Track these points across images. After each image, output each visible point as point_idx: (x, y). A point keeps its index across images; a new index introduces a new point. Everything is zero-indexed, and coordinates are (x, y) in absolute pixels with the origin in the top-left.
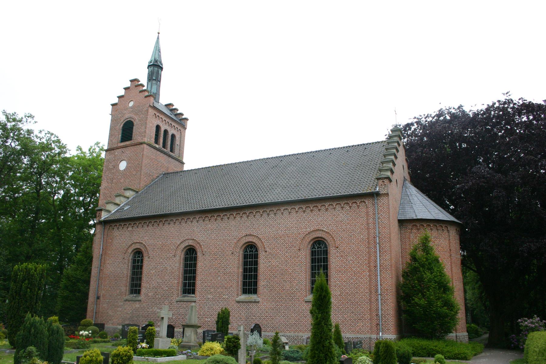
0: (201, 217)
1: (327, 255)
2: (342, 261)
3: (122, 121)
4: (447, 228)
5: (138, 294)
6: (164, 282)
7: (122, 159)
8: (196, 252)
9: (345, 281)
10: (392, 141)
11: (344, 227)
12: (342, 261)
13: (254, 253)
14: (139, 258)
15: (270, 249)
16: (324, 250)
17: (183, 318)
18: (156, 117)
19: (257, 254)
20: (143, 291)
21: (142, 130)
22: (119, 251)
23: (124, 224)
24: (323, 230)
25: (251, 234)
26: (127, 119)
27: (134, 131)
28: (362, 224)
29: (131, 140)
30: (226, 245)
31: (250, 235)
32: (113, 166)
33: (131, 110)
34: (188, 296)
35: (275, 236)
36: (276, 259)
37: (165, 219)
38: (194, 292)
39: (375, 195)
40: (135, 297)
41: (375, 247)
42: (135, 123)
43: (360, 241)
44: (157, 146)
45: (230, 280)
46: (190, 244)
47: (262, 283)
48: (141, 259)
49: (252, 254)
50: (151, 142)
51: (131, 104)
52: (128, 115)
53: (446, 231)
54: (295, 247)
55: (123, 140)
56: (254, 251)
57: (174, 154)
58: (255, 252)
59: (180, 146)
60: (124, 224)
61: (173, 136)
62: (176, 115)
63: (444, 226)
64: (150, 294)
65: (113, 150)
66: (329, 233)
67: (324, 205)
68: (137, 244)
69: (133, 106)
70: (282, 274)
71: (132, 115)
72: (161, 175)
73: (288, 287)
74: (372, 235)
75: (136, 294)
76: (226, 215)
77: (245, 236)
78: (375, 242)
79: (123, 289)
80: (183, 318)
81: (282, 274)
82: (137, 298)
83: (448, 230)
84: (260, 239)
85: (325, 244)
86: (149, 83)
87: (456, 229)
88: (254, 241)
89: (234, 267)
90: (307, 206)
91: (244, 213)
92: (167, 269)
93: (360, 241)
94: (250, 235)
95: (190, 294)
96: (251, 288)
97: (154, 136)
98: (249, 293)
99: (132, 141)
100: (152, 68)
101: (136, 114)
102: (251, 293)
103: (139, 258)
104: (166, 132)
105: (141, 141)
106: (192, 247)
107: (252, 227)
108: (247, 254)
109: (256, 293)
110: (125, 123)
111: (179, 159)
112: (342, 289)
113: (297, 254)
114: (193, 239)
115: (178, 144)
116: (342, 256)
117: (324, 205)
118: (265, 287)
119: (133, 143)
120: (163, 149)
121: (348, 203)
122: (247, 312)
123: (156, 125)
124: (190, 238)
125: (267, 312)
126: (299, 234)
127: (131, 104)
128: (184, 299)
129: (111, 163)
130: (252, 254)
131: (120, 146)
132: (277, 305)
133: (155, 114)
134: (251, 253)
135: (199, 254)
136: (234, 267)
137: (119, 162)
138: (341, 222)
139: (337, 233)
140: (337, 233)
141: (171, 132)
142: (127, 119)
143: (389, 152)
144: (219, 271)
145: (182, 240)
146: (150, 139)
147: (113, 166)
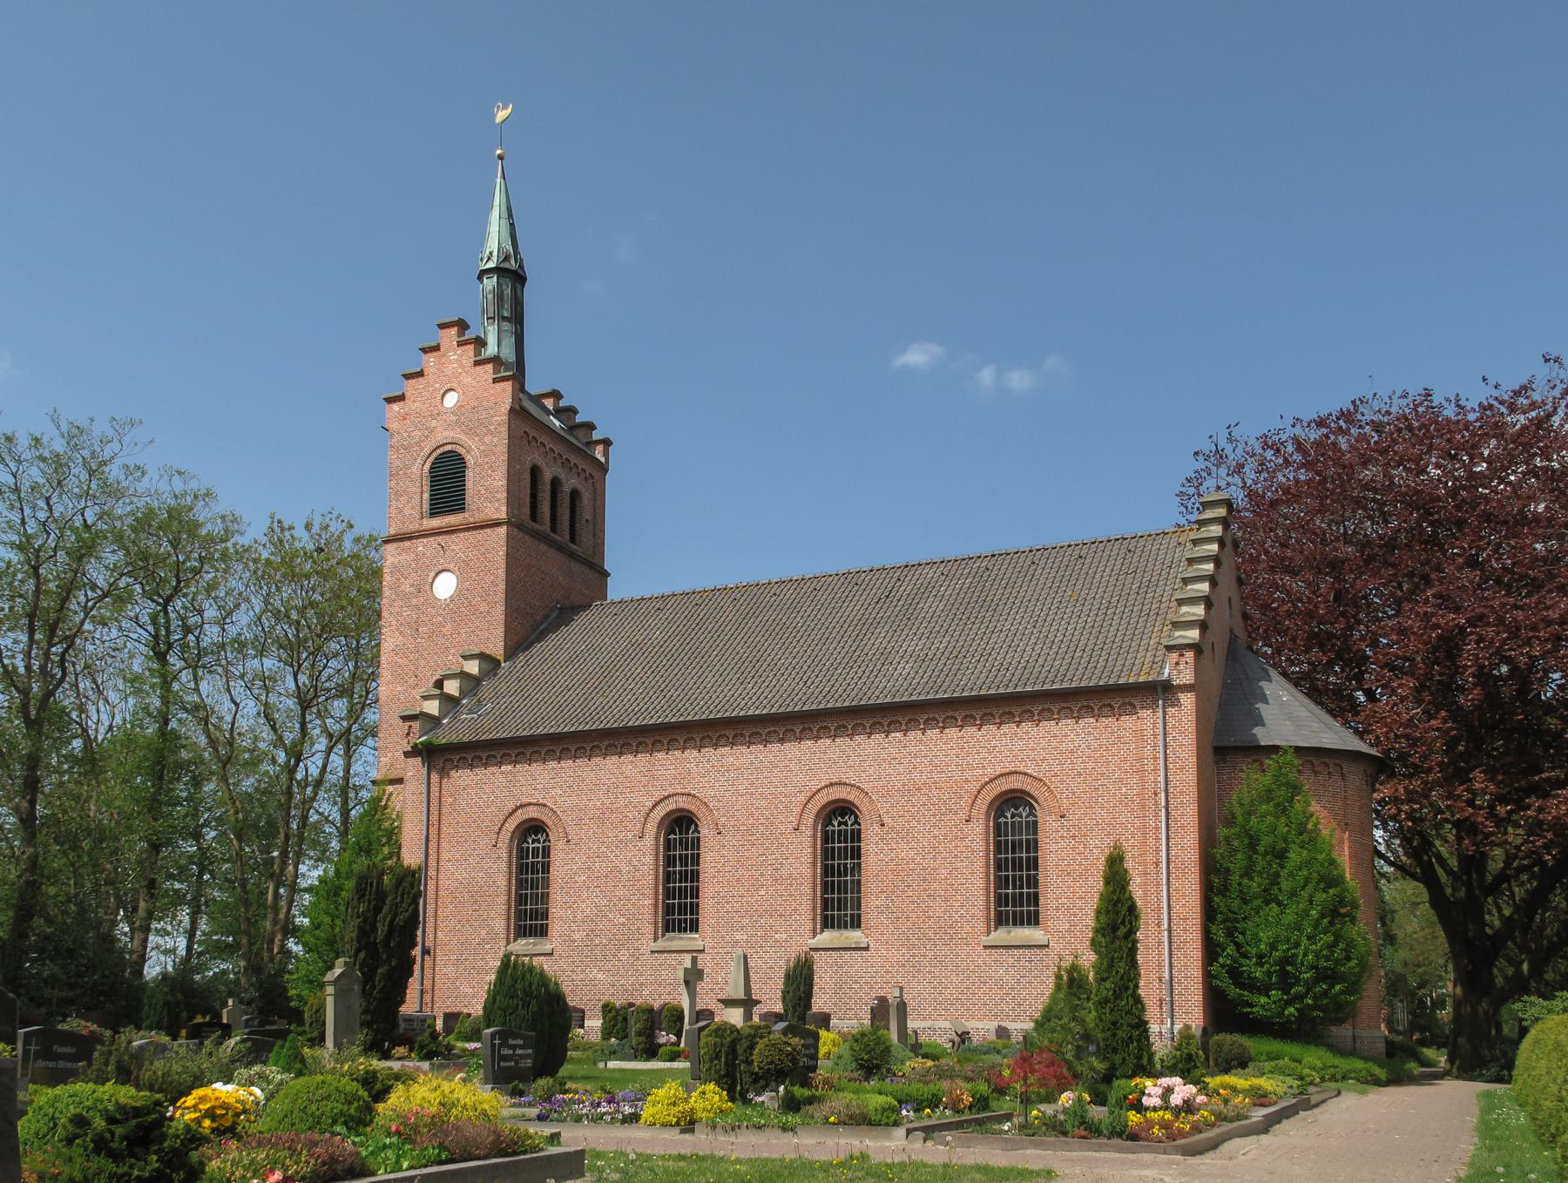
0: (708, 736)
1: (1035, 833)
2: (1073, 849)
3: (427, 450)
4: (1342, 769)
5: (541, 935)
6: (615, 905)
7: (440, 568)
8: (696, 826)
9: (1080, 898)
10: (1204, 535)
11: (1079, 767)
12: (1073, 849)
13: (849, 828)
14: (536, 845)
15: (893, 818)
16: (1027, 823)
17: (669, 993)
18: (529, 442)
19: (859, 831)
20: (556, 927)
21: (495, 483)
22: (478, 827)
23: (489, 756)
24: (1025, 774)
25: (844, 780)
26: (443, 445)
27: (469, 484)
28: (1125, 760)
29: (462, 510)
30: (776, 808)
31: (840, 784)
32: (412, 585)
33: (454, 418)
34: (681, 938)
35: (904, 785)
36: (908, 842)
37: (606, 743)
38: (694, 927)
39: (1159, 689)
40: (534, 944)
41: (1157, 816)
42: (470, 460)
43: (1121, 802)
44: (537, 526)
45: (791, 895)
46: (681, 805)
47: (872, 902)
48: (544, 848)
49: (846, 831)
50: (523, 517)
51: (451, 400)
52: (446, 434)
53: (1336, 777)
54: (956, 813)
55: (437, 509)
56: (849, 823)
57: (580, 550)
58: (852, 825)
59: (594, 524)
60: (489, 756)
61: (575, 495)
62: (573, 428)
63: (1331, 762)
64: (576, 936)
65: (410, 538)
66: (1041, 780)
67: (1029, 711)
68: (531, 808)
69: (458, 408)
70: (925, 880)
71: (450, 435)
72: (552, 610)
73: (939, 912)
74: (1150, 786)
75: (536, 935)
76: (775, 732)
77: (826, 786)
78: (1156, 804)
79: (500, 925)
80: (669, 993)
81: (925, 880)
82: (538, 947)
83: (1342, 774)
84: (867, 793)
85: (1032, 807)
86: (491, 328)
87: (1365, 771)
88: (851, 798)
89: (801, 863)
90: (985, 711)
91: (821, 728)
92: (620, 872)
93: (1121, 802)
94: (840, 784)
95: (685, 931)
96: (846, 915)
97: (528, 500)
98: (839, 927)
99: (466, 515)
100: (495, 279)
101: (470, 432)
102: (846, 927)
103: (536, 845)
104: (555, 483)
105: (495, 516)
106: (685, 814)
107: (845, 763)
108: (833, 831)
109: (859, 926)
110: (436, 459)
111: (595, 561)
112: (1075, 915)
113: (962, 830)
114: (689, 795)
115: (588, 516)
116: (1074, 837)
117: (1029, 711)
118: (882, 912)
119: (471, 520)
120: (551, 534)
121: (1091, 708)
122: (836, 973)
123: (531, 465)
124: (679, 791)
125: (887, 972)
126: (967, 781)
127: (451, 400)
128: (670, 946)
129: (406, 578)
130: (846, 831)
131: (430, 527)
132: (914, 956)
133: (525, 432)
134: (843, 827)
135: (704, 831)
136: (801, 863)
137: (433, 574)
138: (1072, 752)
139: (1062, 781)
140: (1062, 781)
141: (570, 483)
142: (443, 445)
143: (1197, 569)
144: (762, 875)
145: (657, 796)
146: (519, 509)
147: (412, 585)
